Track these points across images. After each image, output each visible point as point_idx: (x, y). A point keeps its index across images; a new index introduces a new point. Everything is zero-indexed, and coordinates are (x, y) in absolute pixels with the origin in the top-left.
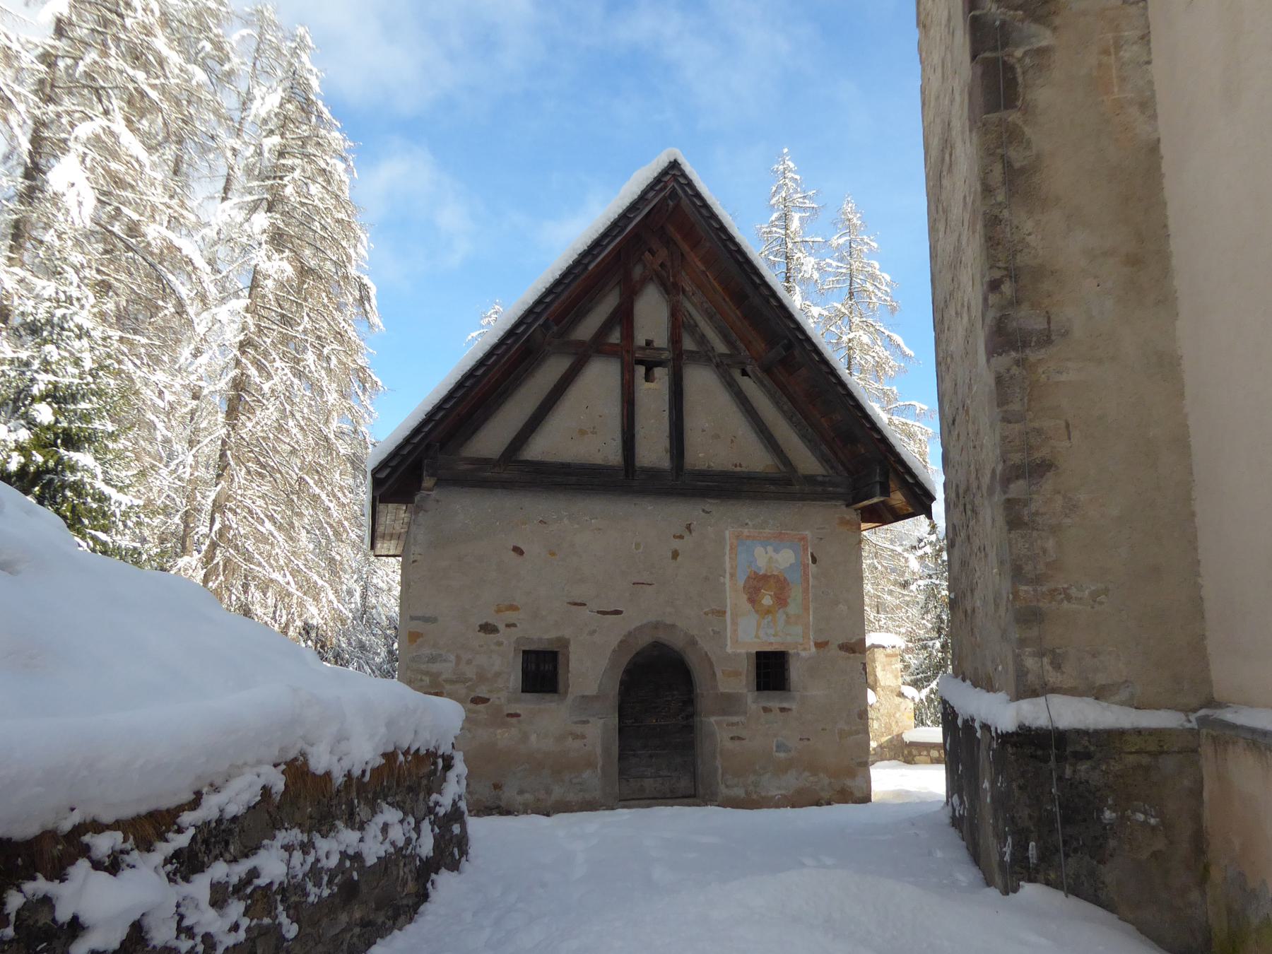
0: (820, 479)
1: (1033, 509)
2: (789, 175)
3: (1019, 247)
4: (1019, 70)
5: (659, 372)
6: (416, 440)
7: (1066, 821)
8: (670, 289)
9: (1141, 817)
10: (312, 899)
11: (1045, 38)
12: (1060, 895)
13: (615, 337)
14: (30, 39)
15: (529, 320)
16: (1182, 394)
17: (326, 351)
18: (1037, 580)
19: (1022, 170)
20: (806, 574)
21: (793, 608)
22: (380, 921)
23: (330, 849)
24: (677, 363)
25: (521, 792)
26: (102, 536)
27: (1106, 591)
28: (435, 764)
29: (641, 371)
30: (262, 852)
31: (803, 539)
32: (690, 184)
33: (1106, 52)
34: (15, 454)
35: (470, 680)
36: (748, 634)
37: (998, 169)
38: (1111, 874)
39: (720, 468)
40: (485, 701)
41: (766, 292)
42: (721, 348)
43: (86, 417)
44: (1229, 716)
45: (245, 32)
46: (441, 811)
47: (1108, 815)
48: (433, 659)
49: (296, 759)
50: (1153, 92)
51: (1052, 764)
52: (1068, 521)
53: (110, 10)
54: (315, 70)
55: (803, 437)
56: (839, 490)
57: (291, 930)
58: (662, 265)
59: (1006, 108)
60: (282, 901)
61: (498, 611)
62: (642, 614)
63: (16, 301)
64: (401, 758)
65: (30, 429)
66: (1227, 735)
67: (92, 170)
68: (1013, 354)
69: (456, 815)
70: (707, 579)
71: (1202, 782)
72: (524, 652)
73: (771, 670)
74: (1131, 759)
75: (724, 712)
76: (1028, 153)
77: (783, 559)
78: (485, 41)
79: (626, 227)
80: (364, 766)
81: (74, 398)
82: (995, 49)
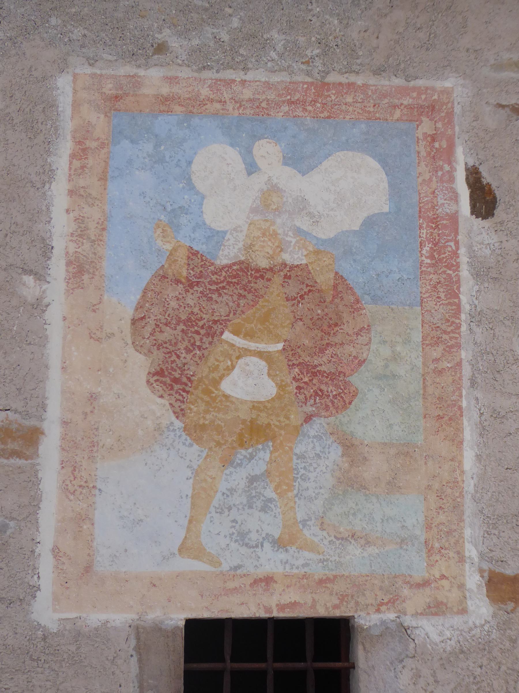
20: (442, 259)
21: (376, 415)
31: (432, 108)
77: (335, 196)
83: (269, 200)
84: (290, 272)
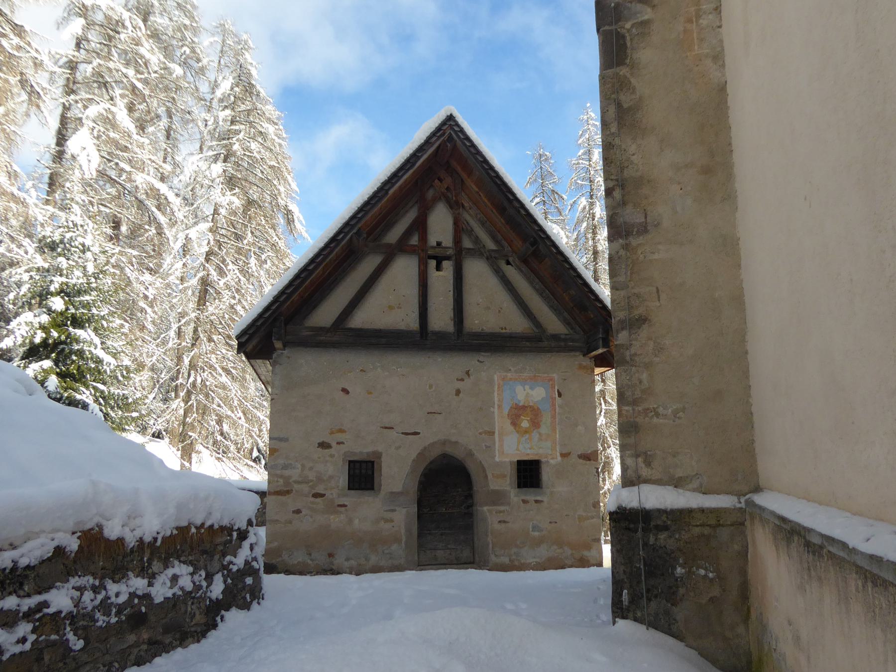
0: (563, 337)
1: (633, 352)
2: (591, 122)
3: (626, 165)
4: (628, 38)
5: (446, 264)
6: (266, 315)
7: (650, 574)
8: (454, 206)
9: (702, 572)
10: (100, 623)
11: (647, 14)
12: (643, 628)
13: (414, 240)
14: (59, 51)
15: (346, 230)
16: (739, 265)
17: (263, 257)
18: (635, 403)
19: (629, 109)
20: (553, 405)
21: (544, 430)
22: (167, 641)
23: (119, 591)
24: (458, 257)
25: (347, 559)
26: (101, 387)
27: (683, 410)
28: (231, 535)
29: (433, 263)
30: (54, 592)
31: (551, 379)
32: (462, 131)
33: (690, 21)
34: (39, 332)
35: (312, 481)
36: (512, 447)
37: (612, 110)
38: (680, 613)
39: (491, 331)
40: (322, 495)
41: (517, 205)
42: (491, 245)
43: (87, 306)
44: (761, 499)
45: (212, 40)
46: (235, 568)
47: (679, 571)
48: (285, 467)
49: (92, 529)
50: (722, 47)
51: (640, 534)
52: (657, 359)
53: (111, 30)
54: (254, 63)
55: (551, 307)
56: (577, 344)
57: (77, 644)
58: (448, 189)
59: (618, 65)
60: (70, 624)
61: (332, 433)
62: (433, 434)
63: (39, 229)
64: (193, 530)
65: (49, 315)
66: (756, 512)
67: (98, 138)
68: (621, 241)
69: (249, 569)
70: (481, 409)
71: (747, 547)
72: (350, 462)
73: (528, 474)
74: (697, 530)
75: (494, 503)
76: (633, 97)
77: (537, 394)
78: (404, 37)
79: (416, 162)
80: (155, 535)
81: (79, 293)
82: (611, 24)
83: (527, 395)
84: (531, 407)
